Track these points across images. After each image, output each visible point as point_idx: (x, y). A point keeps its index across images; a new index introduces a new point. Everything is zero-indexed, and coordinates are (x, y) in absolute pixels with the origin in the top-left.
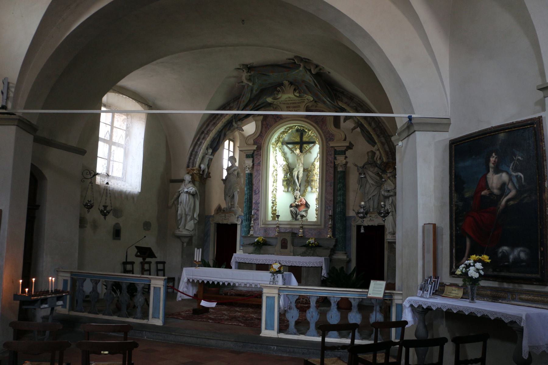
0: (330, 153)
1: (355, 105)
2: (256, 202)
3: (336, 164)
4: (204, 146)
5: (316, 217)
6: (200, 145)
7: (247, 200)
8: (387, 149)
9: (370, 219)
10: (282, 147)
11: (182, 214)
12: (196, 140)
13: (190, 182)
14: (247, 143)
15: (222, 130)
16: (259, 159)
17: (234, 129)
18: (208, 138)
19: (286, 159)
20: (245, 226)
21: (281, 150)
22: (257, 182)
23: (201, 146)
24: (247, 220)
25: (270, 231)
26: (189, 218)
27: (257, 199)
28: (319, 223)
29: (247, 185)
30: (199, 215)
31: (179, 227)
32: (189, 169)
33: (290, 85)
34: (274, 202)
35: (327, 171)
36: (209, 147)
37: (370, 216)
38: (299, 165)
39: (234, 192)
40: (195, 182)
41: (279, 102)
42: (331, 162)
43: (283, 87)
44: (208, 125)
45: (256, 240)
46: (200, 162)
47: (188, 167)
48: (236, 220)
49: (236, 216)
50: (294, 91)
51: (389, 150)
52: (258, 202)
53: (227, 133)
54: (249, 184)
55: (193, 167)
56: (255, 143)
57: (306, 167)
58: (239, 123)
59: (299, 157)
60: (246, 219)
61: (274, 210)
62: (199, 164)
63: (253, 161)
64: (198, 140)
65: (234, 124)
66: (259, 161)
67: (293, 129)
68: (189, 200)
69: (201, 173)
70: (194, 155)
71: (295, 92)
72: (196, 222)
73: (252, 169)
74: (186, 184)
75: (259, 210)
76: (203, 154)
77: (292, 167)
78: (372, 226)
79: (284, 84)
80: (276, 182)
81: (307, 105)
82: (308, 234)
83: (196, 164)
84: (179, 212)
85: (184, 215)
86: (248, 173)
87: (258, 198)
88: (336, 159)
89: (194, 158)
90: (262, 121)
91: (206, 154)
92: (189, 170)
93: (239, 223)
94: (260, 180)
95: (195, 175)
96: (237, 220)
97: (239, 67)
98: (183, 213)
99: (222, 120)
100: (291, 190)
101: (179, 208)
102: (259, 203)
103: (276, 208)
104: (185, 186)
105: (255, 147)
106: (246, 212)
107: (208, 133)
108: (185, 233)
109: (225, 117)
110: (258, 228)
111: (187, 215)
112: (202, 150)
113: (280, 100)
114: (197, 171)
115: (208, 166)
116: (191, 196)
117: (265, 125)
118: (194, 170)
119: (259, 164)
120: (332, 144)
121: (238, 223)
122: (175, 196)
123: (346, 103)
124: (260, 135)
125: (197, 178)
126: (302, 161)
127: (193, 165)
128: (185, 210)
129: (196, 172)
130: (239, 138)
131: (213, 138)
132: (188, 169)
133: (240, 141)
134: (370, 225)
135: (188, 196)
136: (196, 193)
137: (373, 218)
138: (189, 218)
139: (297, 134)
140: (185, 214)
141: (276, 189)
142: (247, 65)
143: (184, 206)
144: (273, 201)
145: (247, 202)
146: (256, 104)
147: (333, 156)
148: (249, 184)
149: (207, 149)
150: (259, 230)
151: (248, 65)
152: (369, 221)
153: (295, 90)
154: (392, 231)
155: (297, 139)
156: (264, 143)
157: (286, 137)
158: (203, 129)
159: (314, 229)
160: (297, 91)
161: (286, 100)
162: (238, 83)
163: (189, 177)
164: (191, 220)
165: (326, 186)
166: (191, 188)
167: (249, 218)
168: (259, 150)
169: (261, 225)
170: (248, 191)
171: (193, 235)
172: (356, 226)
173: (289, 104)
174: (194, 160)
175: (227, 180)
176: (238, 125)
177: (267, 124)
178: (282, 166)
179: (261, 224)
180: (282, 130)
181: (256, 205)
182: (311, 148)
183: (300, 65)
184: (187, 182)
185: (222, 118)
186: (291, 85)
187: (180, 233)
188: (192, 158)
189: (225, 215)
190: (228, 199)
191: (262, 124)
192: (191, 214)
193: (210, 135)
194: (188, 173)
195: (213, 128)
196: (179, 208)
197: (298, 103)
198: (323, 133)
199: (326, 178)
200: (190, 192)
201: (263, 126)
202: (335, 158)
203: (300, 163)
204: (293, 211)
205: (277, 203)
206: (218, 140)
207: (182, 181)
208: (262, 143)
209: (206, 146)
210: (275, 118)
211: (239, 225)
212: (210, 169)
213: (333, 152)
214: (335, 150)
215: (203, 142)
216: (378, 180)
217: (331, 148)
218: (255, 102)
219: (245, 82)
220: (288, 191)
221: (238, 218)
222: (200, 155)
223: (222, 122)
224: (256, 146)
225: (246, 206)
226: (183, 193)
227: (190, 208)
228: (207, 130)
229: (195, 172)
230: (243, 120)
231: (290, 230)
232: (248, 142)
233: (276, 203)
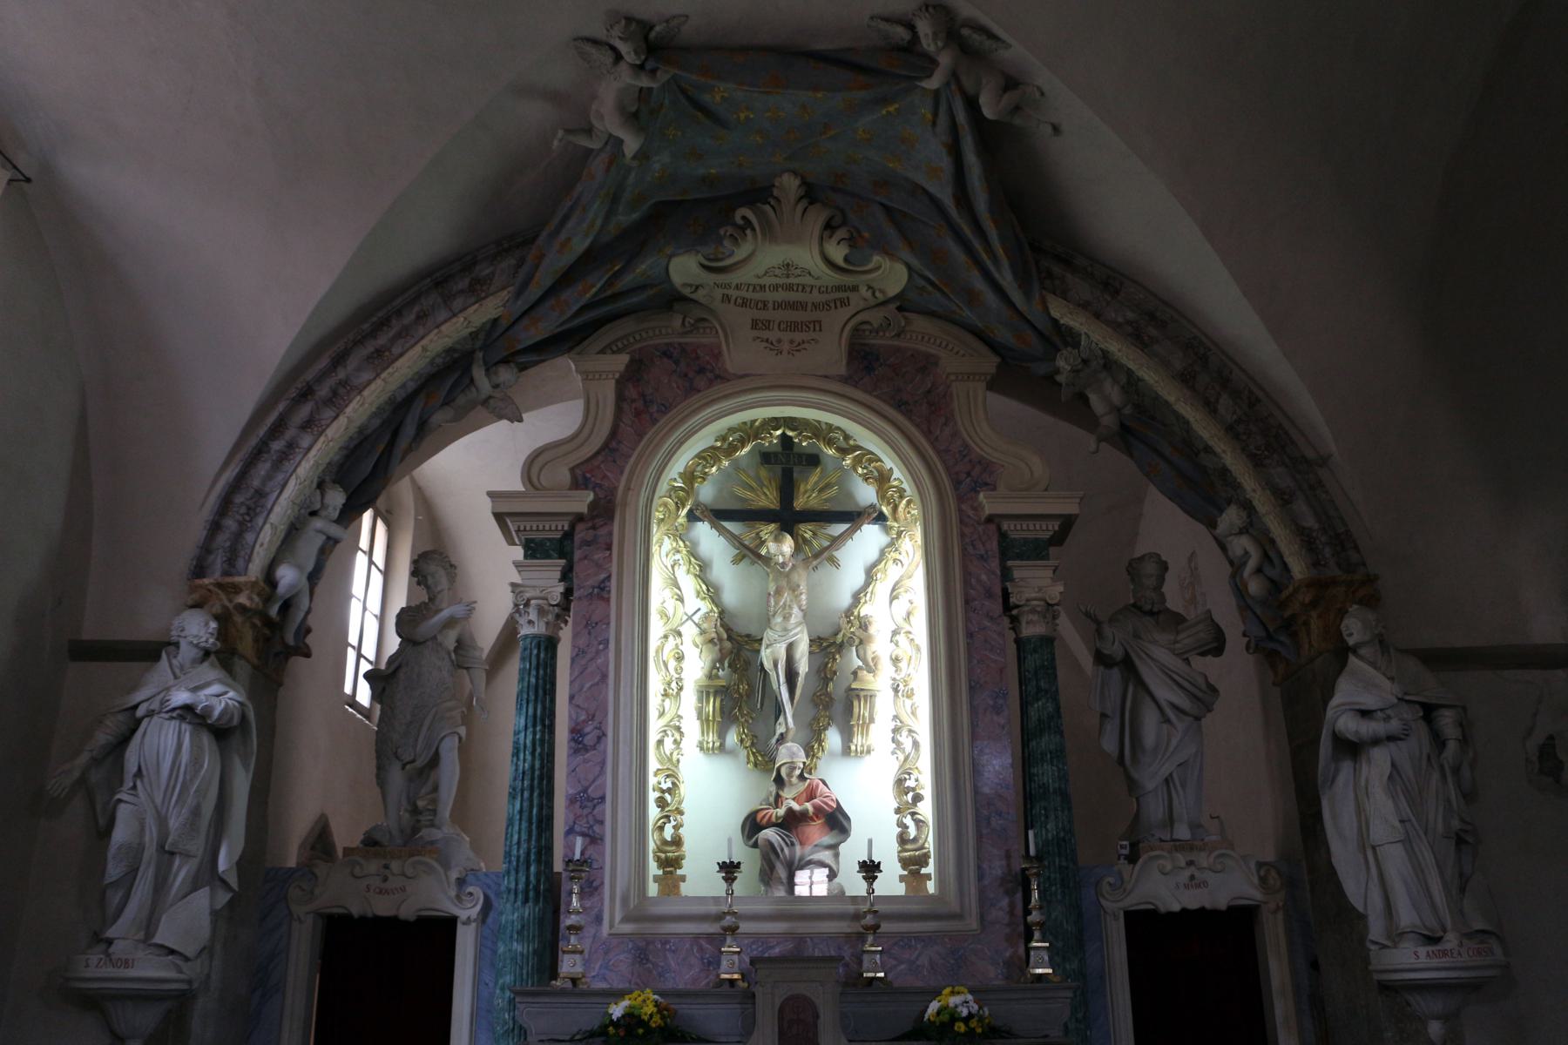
0: (983, 552)
1: (1130, 315)
2: (585, 790)
3: (1013, 600)
4: (307, 467)
5: (902, 879)
6: (284, 456)
7: (532, 780)
8: (1310, 522)
9: (1192, 877)
10: (688, 529)
11: (141, 848)
12: (262, 431)
13: (207, 654)
14: (535, 480)
15: (409, 400)
16: (599, 566)
17: (472, 405)
18: (335, 425)
19: (712, 592)
20: (517, 926)
21: (686, 546)
22: (588, 685)
23: (289, 466)
24: (531, 894)
25: (669, 955)
26: (182, 873)
27: (591, 777)
28: (954, 906)
29: (532, 697)
30: (244, 864)
31: (110, 933)
32: (206, 581)
33: (804, 203)
35: (970, 635)
36: (327, 479)
37: (1190, 863)
38: (786, 618)
39: (443, 738)
40: (236, 659)
41: (719, 293)
42: (989, 594)
43: (767, 208)
44: (339, 360)
45: (617, 1011)
46: (274, 549)
47: (199, 570)
48: (453, 893)
49: (454, 875)
50: (827, 233)
51: (1316, 526)
52: (598, 794)
53: (438, 417)
54: (541, 692)
55: (226, 573)
56: (579, 481)
57: (824, 631)
58: (505, 374)
59: (788, 575)
60: (521, 886)
61: (665, 842)
62: (267, 562)
63: (566, 575)
64: (277, 429)
65: (478, 373)
66: (603, 576)
68: (196, 761)
69: (274, 611)
70: (243, 510)
71: (831, 237)
72: (223, 898)
73: (558, 616)
74: (182, 668)
75: (602, 839)
76: (297, 508)
77: (742, 627)
78: (1202, 910)
79: (776, 192)
80: (678, 694)
81: (859, 318)
82: (895, 966)
83: (249, 560)
84: (121, 833)
85: (150, 851)
86: (535, 637)
87: (598, 768)
88: (1012, 580)
89: (243, 527)
90: (618, 382)
91: (314, 514)
92: (201, 586)
93: (468, 912)
94: (605, 677)
95: (238, 619)
96: (458, 897)
97: (599, 32)
98: (147, 839)
99: (422, 338)
100: (742, 741)
101: (122, 806)
102: (603, 798)
103: (681, 830)
104: (176, 677)
105: (581, 502)
106: (524, 846)
107: (336, 400)
108: (149, 969)
109: (443, 328)
110: (594, 937)
111: (172, 854)
112: (292, 483)
113: (734, 278)
114: (256, 599)
115: (314, 577)
116: (206, 740)
117: (633, 401)
118: (236, 589)
119: (601, 592)
120: (988, 504)
121: (462, 914)
122: (102, 738)
123: (1084, 306)
124: (606, 446)
125: (247, 644)
126: (804, 597)
127: (231, 561)
128: (162, 821)
129: (250, 599)
130: (413, 512)
131: (361, 430)
132: (199, 582)
133: (415, 530)
134: (1193, 905)
135: (191, 735)
136: (244, 718)
137: (1201, 869)
138: (182, 873)
139: (763, 473)
140: (161, 847)
141: (678, 729)
142: (646, 27)
143: (158, 801)
144: (663, 791)
145: (526, 794)
146: (617, 275)
147: (995, 564)
148: (541, 692)
149: (321, 485)
150: (606, 953)
151: (652, 28)
152: (1187, 887)
153: (829, 227)
154: (1418, 922)
156: (628, 489)
157: (706, 492)
158: (310, 375)
159: (927, 940)
160: (842, 233)
161: (762, 281)
162: (568, 131)
163: (207, 624)
164: (195, 885)
165: (973, 710)
166: (216, 688)
167: (538, 881)
168: (599, 521)
169: (614, 921)
170: (534, 733)
171: (195, 985)
172: (1122, 913)
173: (770, 305)
174: (238, 536)
175: (401, 675)
176: (496, 386)
177: (643, 395)
178: (696, 618)
179: (618, 917)
180: (704, 439)
181: (586, 811)
182: (837, 541)
183: (931, 63)
184: (186, 653)
185: (421, 331)
186: (811, 203)
187: (110, 971)
188: (230, 524)
189: (386, 867)
190: (396, 777)
191: (620, 398)
192: (200, 853)
193: (349, 410)
194: (197, 605)
195: (366, 376)
196: (123, 812)
197: (815, 306)
198: (938, 452)
199: (970, 671)
200: (208, 710)
201: (626, 406)
202: (1006, 574)
204: (776, 845)
205: (684, 806)
206: (381, 447)
207: (150, 652)
208: (616, 488)
209: (317, 464)
210: (686, 375)
211: (468, 922)
212: (313, 603)
213: (994, 545)
214: (1003, 536)
215: (305, 443)
216: (1201, 690)
217: (980, 529)
218: (617, 268)
219: (610, 123)
220: (722, 749)
221: (461, 882)
222: (281, 510)
223: (424, 349)
224: (591, 497)
225: (521, 812)
226: (155, 718)
227: (196, 812)
228: (331, 382)
229: (242, 599)
230: (523, 368)
231: (790, 946)
232: (539, 480)
233: (680, 802)
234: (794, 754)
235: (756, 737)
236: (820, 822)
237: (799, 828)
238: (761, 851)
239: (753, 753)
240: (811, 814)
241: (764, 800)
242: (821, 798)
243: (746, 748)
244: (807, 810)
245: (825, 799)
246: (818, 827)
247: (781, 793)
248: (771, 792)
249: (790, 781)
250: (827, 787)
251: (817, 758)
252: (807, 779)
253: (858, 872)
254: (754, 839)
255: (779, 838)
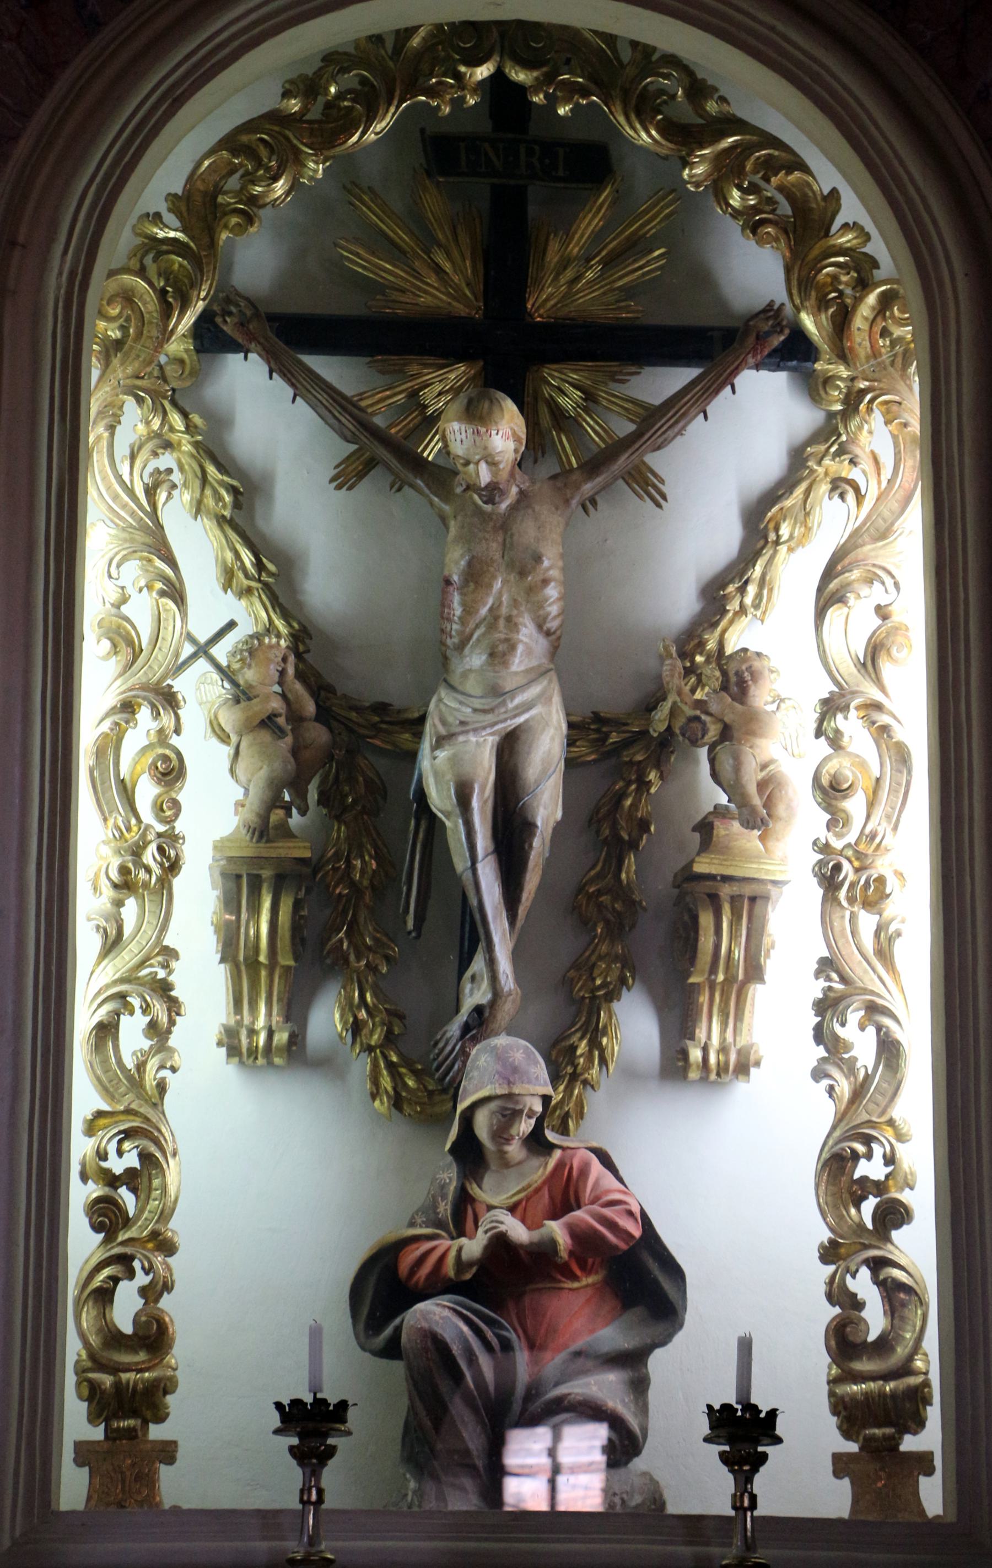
10: (198, 375)
21: (190, 428)
34: (126, 1197)
59: (504, 525)
61: (114, 1338)
67: (431, 92)
100: (356, 1028)
103: (166, 1302)
141: (163, 989)
144: (112, 1181)
155: (438, 270)
203: (511, 623)
204: (456, 1349)
205: (177, 1227)
234: (515, 1070)
235: (401, 1017)
236: (590, 1280)
237: (527, 1300)
238: (410, 1368)
239: (391, 1066)
240: (564, 1254)
241: (422, 1210)
242: (595, 1207)
243: (370, 1049)
244: (553, 1243)
245: (607, 1212)
246: (581, 1298)
247: (474, 1190)
248: (443, 1187)
249: (502, 1154)
250: (621, 1180)
251: (585, 1083)
252: (551, 1147)
253: (707, 1440)
254: (388, 1331)
255: (465, 1329)
